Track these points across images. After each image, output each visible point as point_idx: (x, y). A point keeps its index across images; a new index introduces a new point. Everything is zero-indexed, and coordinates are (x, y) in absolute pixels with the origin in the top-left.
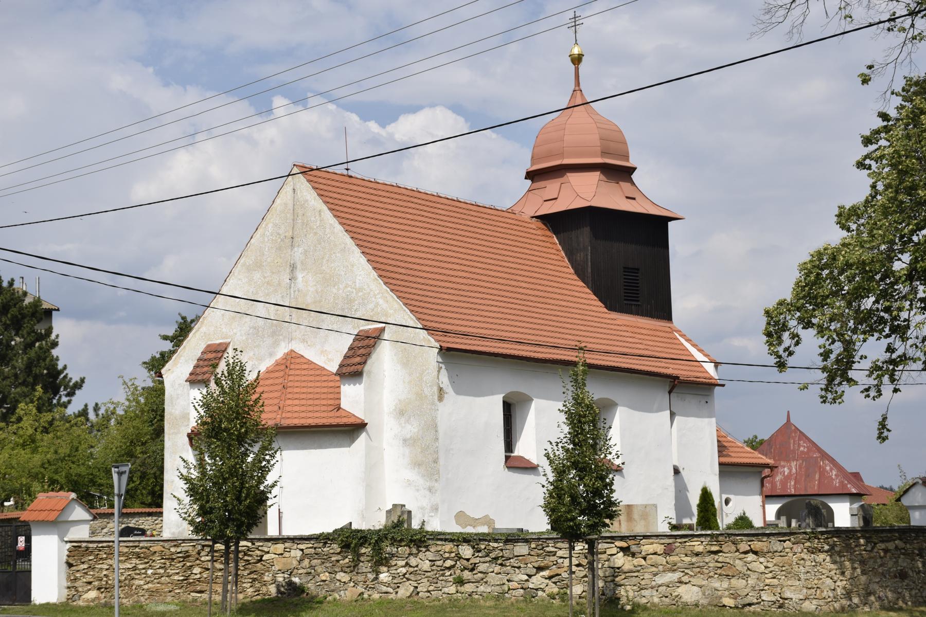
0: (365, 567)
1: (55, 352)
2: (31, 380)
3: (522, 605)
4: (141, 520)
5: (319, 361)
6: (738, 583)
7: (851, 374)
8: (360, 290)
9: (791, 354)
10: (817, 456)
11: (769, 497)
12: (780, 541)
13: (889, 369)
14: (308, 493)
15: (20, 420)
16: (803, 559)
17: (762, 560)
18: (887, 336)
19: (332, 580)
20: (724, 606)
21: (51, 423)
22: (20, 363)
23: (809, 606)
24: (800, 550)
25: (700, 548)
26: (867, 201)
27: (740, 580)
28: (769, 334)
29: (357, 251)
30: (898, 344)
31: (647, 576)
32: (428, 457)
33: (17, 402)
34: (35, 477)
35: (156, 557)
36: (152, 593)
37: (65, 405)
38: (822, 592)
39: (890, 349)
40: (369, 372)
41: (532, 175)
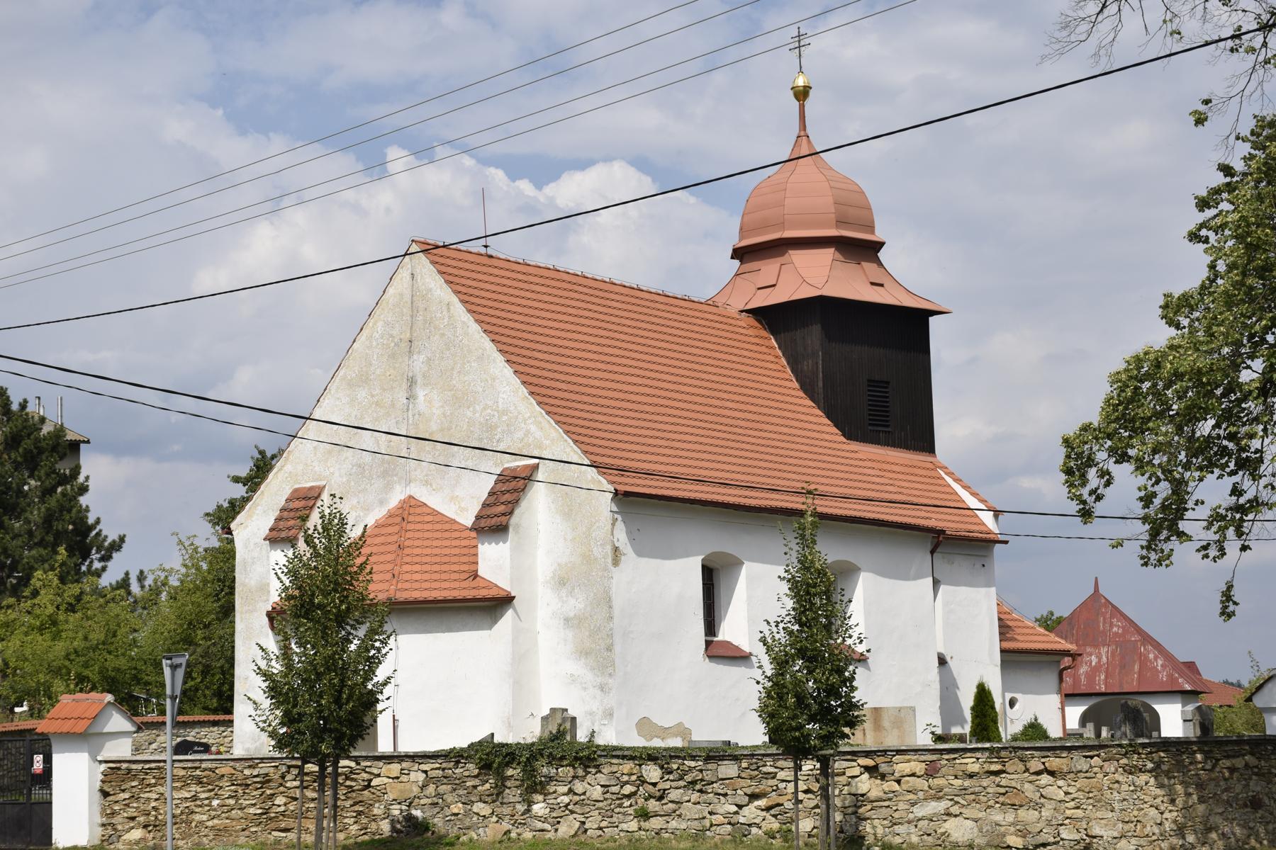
1: (84, 500)
2: (50, 538)
5: (449, 511)
6: (1028, 815)
7: (1183, 526)
8: (505, 412)
9: (1099, 498)
11: (1070, 697)
12: (1086, 757)
14: (435, 694)
15: (35, 593)
16: (1117, 782)
17: (1061, 783)
19: (468, 813)
20: (1009, 847)
21: (79, 598)
22: (36, 515)
24: (1113, 769)
25: (975, 768)
26: (1203, 287)
27: (1031, 812)
28: (1068, 472)
29: (500, 359)
30: (1247, 484)
31: (902, 806)
32: (599, 643)
33: (32, 569)
34: (57, 672)
37: (98, 574)
38: (1145, 827)
39: (1236, 491)
40: (518, 526)
41: (740, 254)
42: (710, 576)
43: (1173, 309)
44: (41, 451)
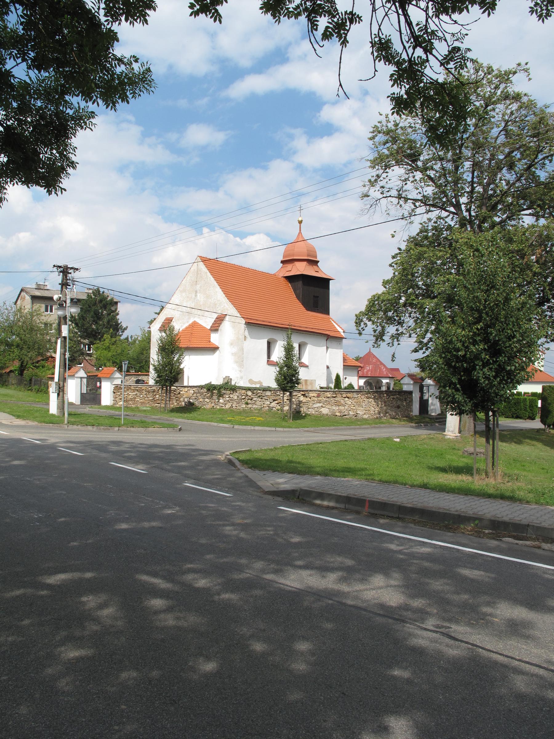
0: (215, 397)
1: (118, 317)
2: (109, 326)
3: (267, 412)
4: (143, 377)
5: (204, 325)
6: (342, 408)
7: (384, 338)
8: (219, 301)
9: (364, 330)
10: (379, 363)
11: (360, 377)
13: (397, 337)
14: (197, 371)
15: (104, 340)
18: (397, 325)
19: (204, 401)
21: (115, 342)
22: (105, 320)
23: (366, 417)
25: (329, 396)
26: (392, 278)
28: (356, 323)
29: (218, 287)
30: (400, 328)
31: (311, 404)
32: (240, 360)
33: (104, 334)
34: (109, 360)
35: (144, 391)
36: (142, 403)
37: (121, 336)
39: (397, 330)
41: (282, 262)
42: (269, 344)
43: (385, 283)
44: (107, 304)
